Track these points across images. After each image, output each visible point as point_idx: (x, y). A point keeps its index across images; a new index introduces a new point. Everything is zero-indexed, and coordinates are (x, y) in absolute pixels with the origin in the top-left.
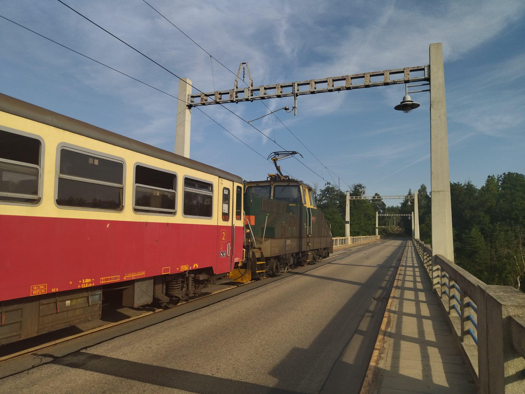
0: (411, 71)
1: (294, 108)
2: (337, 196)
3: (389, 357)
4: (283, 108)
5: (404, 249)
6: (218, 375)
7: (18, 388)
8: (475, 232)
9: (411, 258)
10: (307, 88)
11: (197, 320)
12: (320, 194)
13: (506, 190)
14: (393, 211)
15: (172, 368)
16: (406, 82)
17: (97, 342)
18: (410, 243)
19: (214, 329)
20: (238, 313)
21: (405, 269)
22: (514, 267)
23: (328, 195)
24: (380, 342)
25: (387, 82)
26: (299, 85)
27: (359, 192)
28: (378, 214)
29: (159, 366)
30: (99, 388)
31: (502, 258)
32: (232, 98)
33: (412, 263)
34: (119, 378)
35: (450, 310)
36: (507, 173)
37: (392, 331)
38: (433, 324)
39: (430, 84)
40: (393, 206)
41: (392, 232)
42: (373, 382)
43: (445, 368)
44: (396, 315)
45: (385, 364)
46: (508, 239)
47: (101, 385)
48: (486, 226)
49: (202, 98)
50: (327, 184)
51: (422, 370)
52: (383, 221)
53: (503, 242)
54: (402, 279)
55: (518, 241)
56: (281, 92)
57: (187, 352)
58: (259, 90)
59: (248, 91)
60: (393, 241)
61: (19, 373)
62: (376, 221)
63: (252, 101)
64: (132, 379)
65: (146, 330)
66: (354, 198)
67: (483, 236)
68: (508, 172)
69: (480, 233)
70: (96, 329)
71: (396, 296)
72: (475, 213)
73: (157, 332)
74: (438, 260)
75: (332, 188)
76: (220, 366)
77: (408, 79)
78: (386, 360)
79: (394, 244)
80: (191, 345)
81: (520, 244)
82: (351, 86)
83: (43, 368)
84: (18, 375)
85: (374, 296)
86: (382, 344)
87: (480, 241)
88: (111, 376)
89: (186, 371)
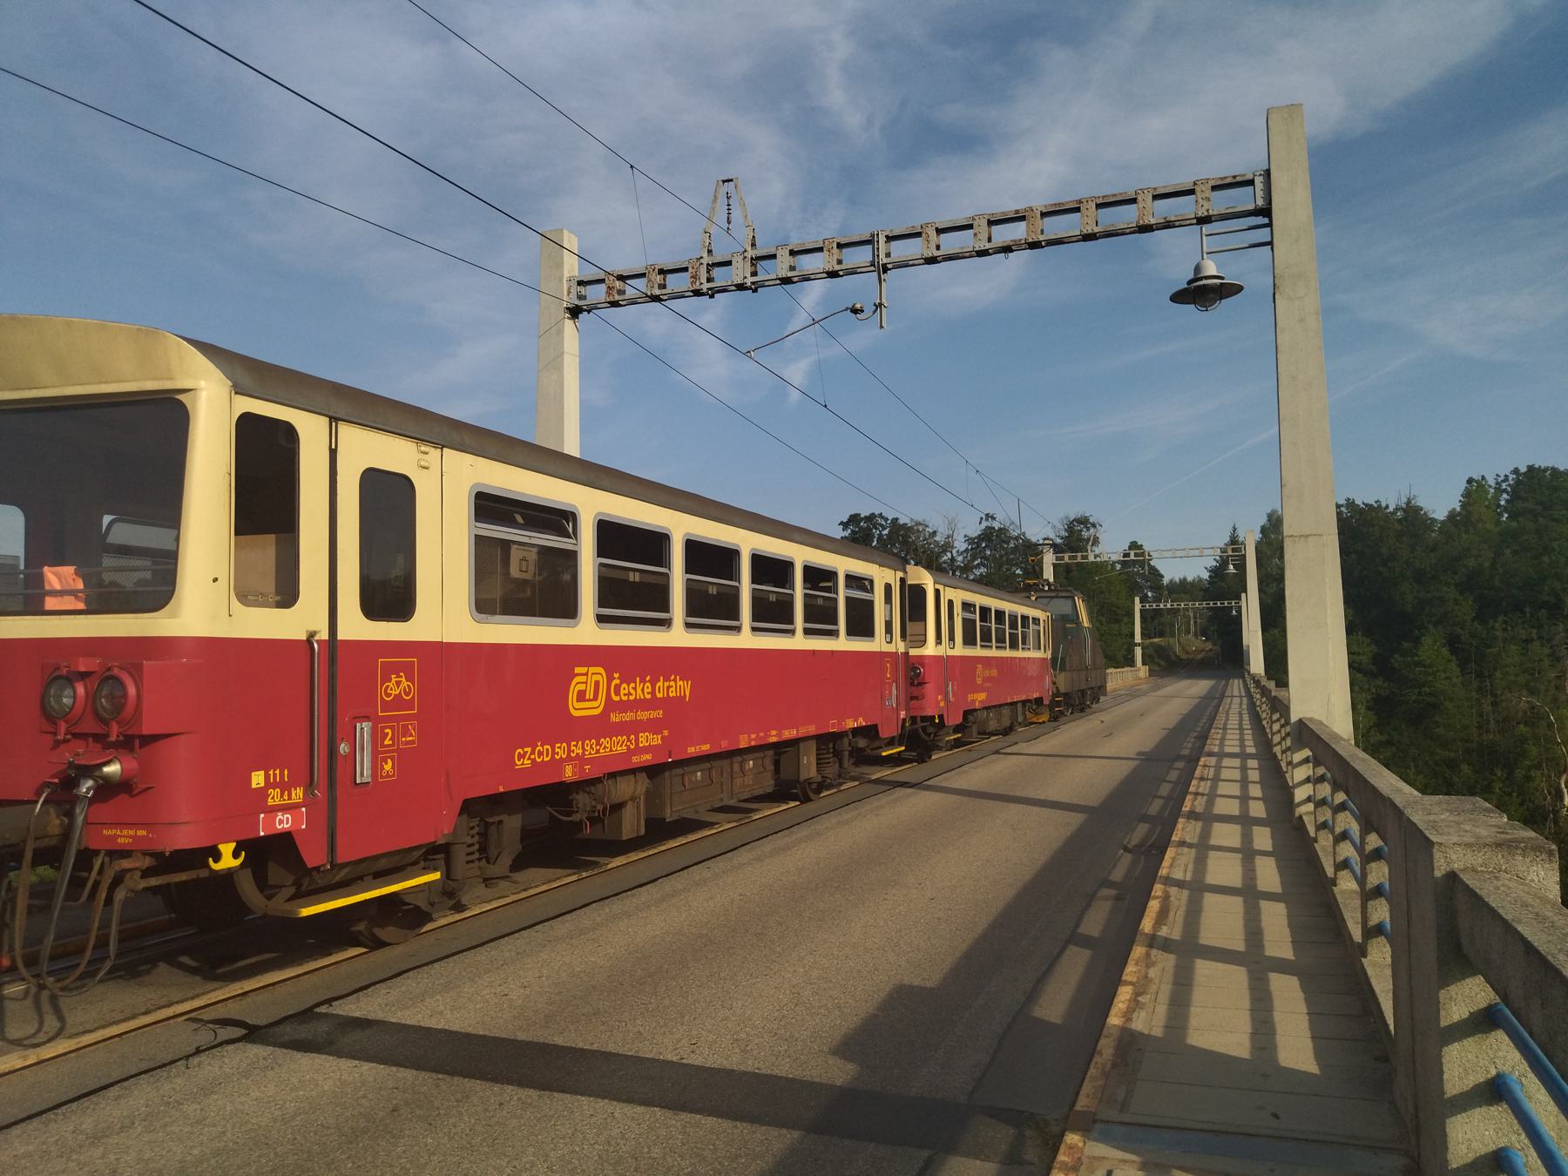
0: (1214, 188)
2: (1015, 555)
3: (1159, 1003)
5: (1218, 706)
6: (696, 1060)
7: (169, 1103)
8: (1431, 647)
9: (1238, 732)
11: (626, 921)
13: (1521, 519)
16: (1203, 221)
18: (1236, 686)
19: (674, 942)
23: (988, 552)
24: (1136, 964)
25: (1146, 222)
26: (889, 239)
27: (1080, 539)
31: (1515, 724)
32: (698, 283)
35: (1335, 874)
36: (1523, 469)
39: (1270, 225)
40: (1185, 579)
41: (1184, 656)
42: (1114, 1066)
44: (1185, 893)
45: (1150, 1021)
46: (1530, 665)
49: (609, 287)
50: (984, 518)
51: (1252, 1033)
53: (1516, 675)
56: (840, 262)
58: (774, 256)
59: (741, 262)
61: (164, 1065)
62: (1134, 624)
64: (465, 1077)
65: (488, 949)
66: (1066, 559)
68: (1528, 466)
69: (1445, 651)
71: (1188, 841)
73: (518, 954)
74: (1305, 734)
75: (1000, 529)
77: (1206, 214)
79: (1189, 691)
82: (1041, 238)
83: (225, 1054)
84: (163, 1073)
86: (1144, 969)
87: (1448, 674)
88: (407, 1070)
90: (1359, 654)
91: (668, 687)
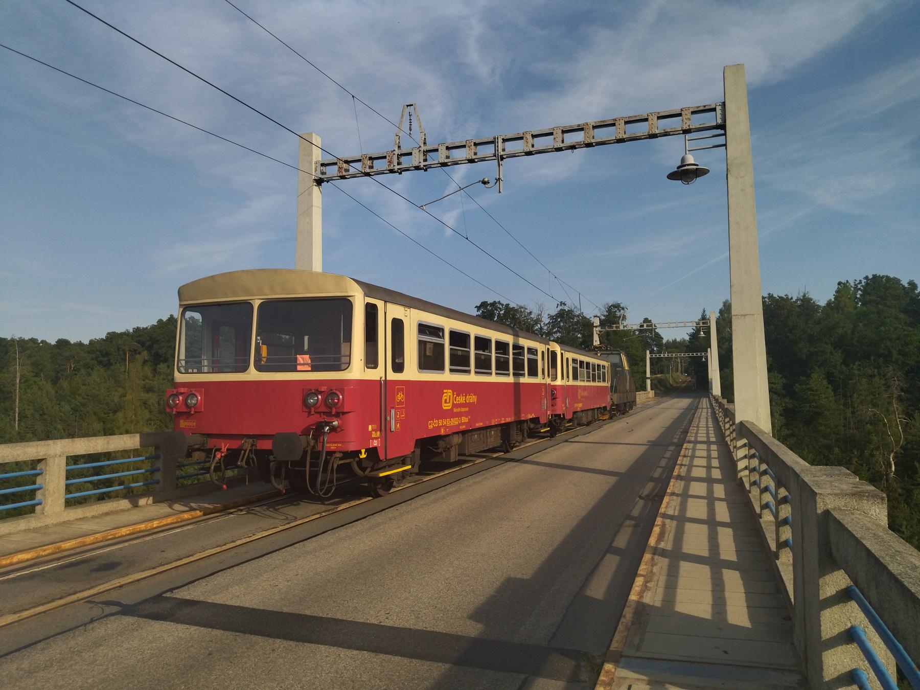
0: (693, 113)
1: (498, 180)
3: (659, 587)
4: (479, 182)
5: (694, 414)
6: (389, 623)
7: (74, 652)
8: (817, 379)
9: (705, 429)
10: (518, 147)
12: (549, 323)
13: (868, 305)
14: (675, 348)
15: (313, 615)
16: (686, 132)
17: (188, 581)
18: (704, 402)
20: (416, 528)
21: (693, 447)
22: (884, 438)
23: (562, 324)
24: (646, 565)
25: (654, 132)
26: (504, 140)
27: (615, 317)
28: (650, 354)
30: (200, 648)
31: (864, 424)
32: (392, 166)
33: (709, 437)
34: (231, 633)
35: (761, 511)
36: (870, 277)
37: (667, 546)
38: (733, 534)
39: (725, 134)
40: (675, 340)
41: (675, 385)
42: (633, 623)
44: (675, 523)
45: (654, 597)
46: (874, 390)
47: (204, 644)
48: (835, 369)
49: (340, 167)
50: (559, 304)
52: (659, 365)
53: (865, 396)
54: (687, 464)
55: (890, 394)
56: (475, 154)
57: (337, 590)
58: (437, 150)
60: (676, 400)
62: (646, 366)
63: (426, 170)
68: (873, 275)
69: (825, 382)
70: (183, 560)
71: (676, 492)
72: (816, 348)
74: (743, 430)
75: (569, 311)
76: (391, 610)
77: (688, 128)
78: (654, 591)
79: (678, 405)
81: (893, 399)
82: (593, 141)
84: (71, 634)
86: (650, 567)
88: (218, 630)
89: (337, 618)
90: (775, 384)
91: (470, 398)
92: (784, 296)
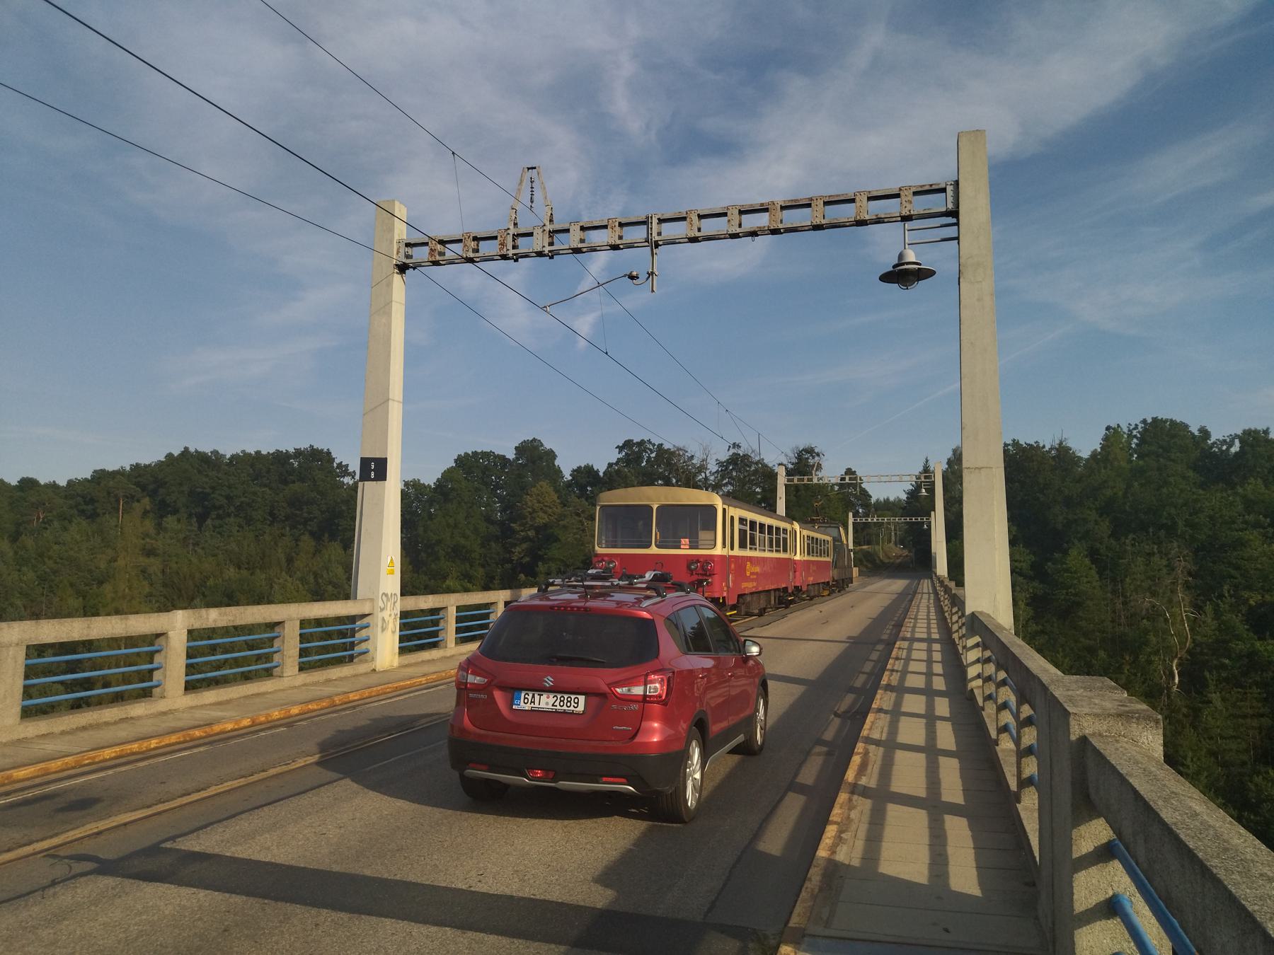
0: (915, 193)
1: (651, 274)
3: (858, 839)
4: (625, 276)
5: (911, 601)
7: (26, 928)
8: (1076, 557)
9: (926, 621)
12: (717, 472)
13: (1146, 459)
14: (889, 510)
16: (906, 218)
18: (926, 585)
23: (734, 474)
24: (841, 808)
25: (862, 218)
26: (661, 221)
27: (808, 466)
28: (853, 517)
29: (347, 871)
32: (505, 249)
33: (927, 633)
35: (998, 736)
36: (1149, 420)
39: (957, 224)
40: (888, 499)
41: (886, 561)
42: (821, 890)
43: (977, 860)
45: (850, 854)
48: (1101, 543)
49: (431, 249)
56: (620, 238)
58: (567, 231)
60: (887, 581)
65: (310, 796)
66: (796, 481)
67: (1094, 566)
68: (1152, 418)
69: (1087, 561)
70: (192, 796)
71: (885, 708)
73: (336, 799)
74: (976, 624)
75: (744, 455)
77: (908, 213)
80: (416, 827)
82: (780, 226)
83: (78, 885)
85: (836, 709)
87: (1089, 579)
92: (1034, 444)
